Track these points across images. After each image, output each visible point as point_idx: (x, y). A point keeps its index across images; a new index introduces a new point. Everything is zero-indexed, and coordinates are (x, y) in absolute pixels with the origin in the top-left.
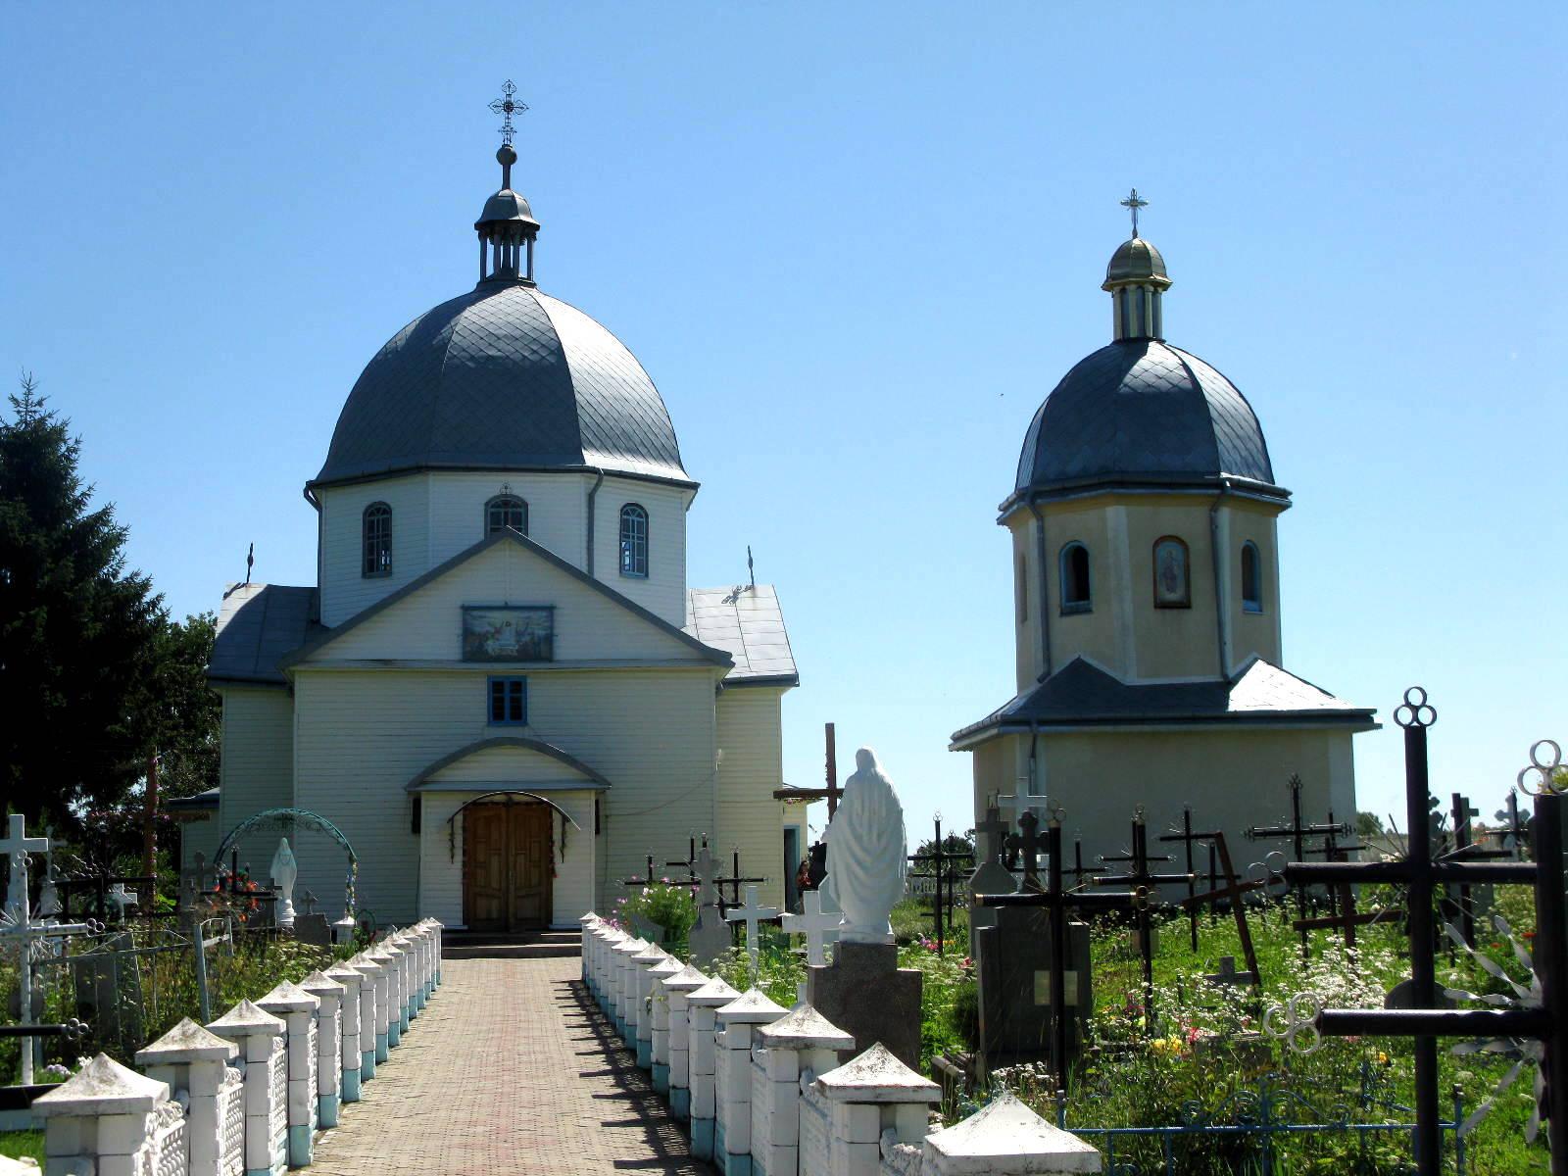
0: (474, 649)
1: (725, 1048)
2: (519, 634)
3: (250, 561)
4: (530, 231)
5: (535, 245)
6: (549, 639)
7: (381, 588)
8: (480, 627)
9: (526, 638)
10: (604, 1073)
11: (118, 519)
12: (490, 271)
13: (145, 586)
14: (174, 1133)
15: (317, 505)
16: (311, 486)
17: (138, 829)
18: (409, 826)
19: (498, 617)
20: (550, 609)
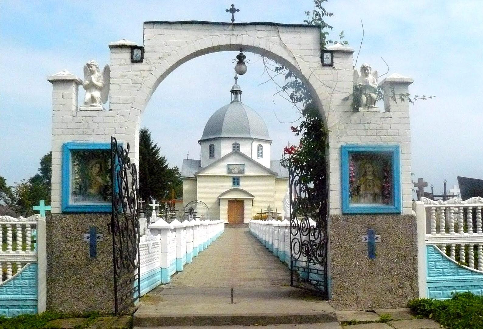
0: (230, 171)
1: (268, 249)
2: (238, 169)
3: (188, 155)
4: (240, 92)
5: (241, 94)
6: (244, 170)
7: (213, 160)
8: (231, 167)
9: (239, 170)
10: (323, 271)
11: (158, 146)
12: (233, 100)
13: (164, 158)
14: (144, 245)
15: (200, 144)
16: (199, 141)
17: (461, 264)
18: (218, 204)
19: (234, 166)
20: (415, 187)
